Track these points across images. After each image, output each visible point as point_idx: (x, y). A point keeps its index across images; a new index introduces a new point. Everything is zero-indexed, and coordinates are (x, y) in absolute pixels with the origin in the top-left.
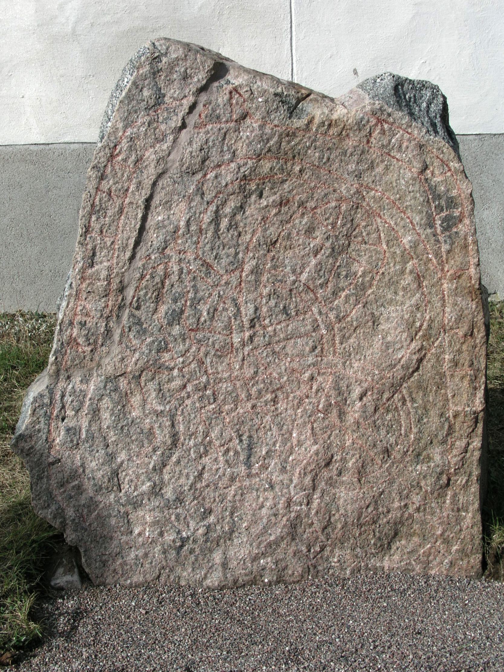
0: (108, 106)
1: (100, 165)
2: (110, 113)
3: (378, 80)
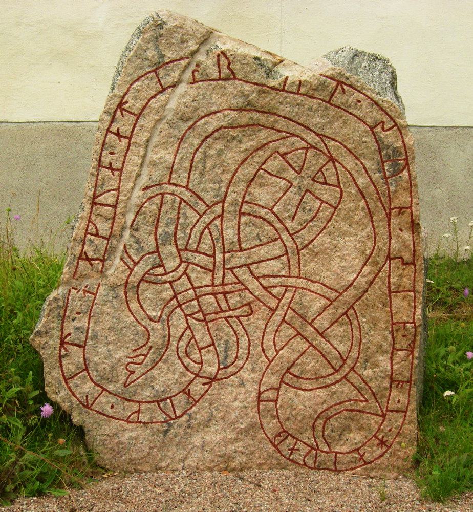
0: (119, 64)
1: (110, 111)
2: (120, 69)
3: (340, 52)
